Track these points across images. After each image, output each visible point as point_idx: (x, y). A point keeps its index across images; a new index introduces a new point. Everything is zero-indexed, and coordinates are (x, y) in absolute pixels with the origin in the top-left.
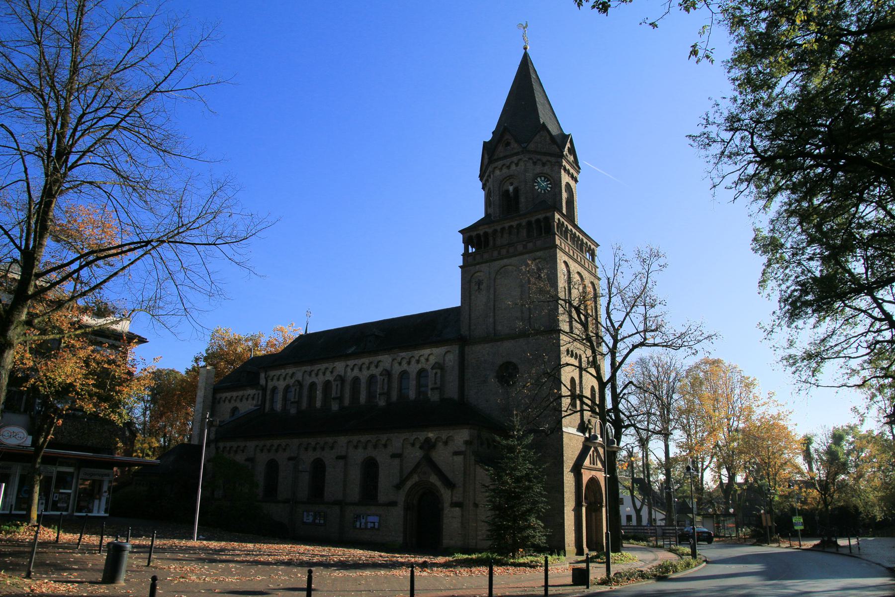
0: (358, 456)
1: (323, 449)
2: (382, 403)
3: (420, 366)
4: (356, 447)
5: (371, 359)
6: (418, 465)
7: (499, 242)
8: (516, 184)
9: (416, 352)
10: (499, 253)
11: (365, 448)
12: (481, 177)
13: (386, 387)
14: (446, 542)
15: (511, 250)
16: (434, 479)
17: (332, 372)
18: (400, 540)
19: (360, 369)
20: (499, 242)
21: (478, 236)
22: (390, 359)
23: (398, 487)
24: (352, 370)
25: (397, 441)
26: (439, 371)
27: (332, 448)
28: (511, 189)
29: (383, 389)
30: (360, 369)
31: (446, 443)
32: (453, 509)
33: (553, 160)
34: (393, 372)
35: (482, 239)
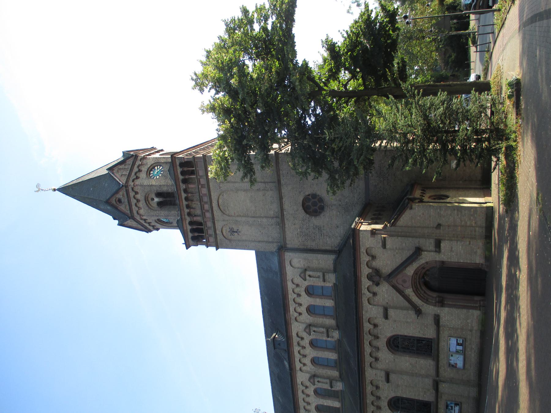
0: (386, 357)
1: (379, 398)
2: (336, 335)
3: (303, 293)
4: (377, 359)
5: (295, 343)
6: (394, 287)
7: (198, 212)
8: (153, 196)
9: (290, 296)
10: (208, 211)
11: (378, 349)
12: (148, 231)
13: (322, 330)
14: (478, 259)
15: (206, 199)
16: (410, 271)
17: (307, 387)
18: (476, 313)
19: (305, 356)
20: (198, 212)
21: (192, 231)
22: (296, 323)
23: (419, 312)
24: (304, 365)
25: (370, 311)
26: (308, 273)
27: (377, 387)
28: (156, 200)
29: (323, 333)
30: (305, 356)
31: (373, 257)
32: (443, 251)
33: (138, 163)
34: (308, 322)
35: (195, 227)
